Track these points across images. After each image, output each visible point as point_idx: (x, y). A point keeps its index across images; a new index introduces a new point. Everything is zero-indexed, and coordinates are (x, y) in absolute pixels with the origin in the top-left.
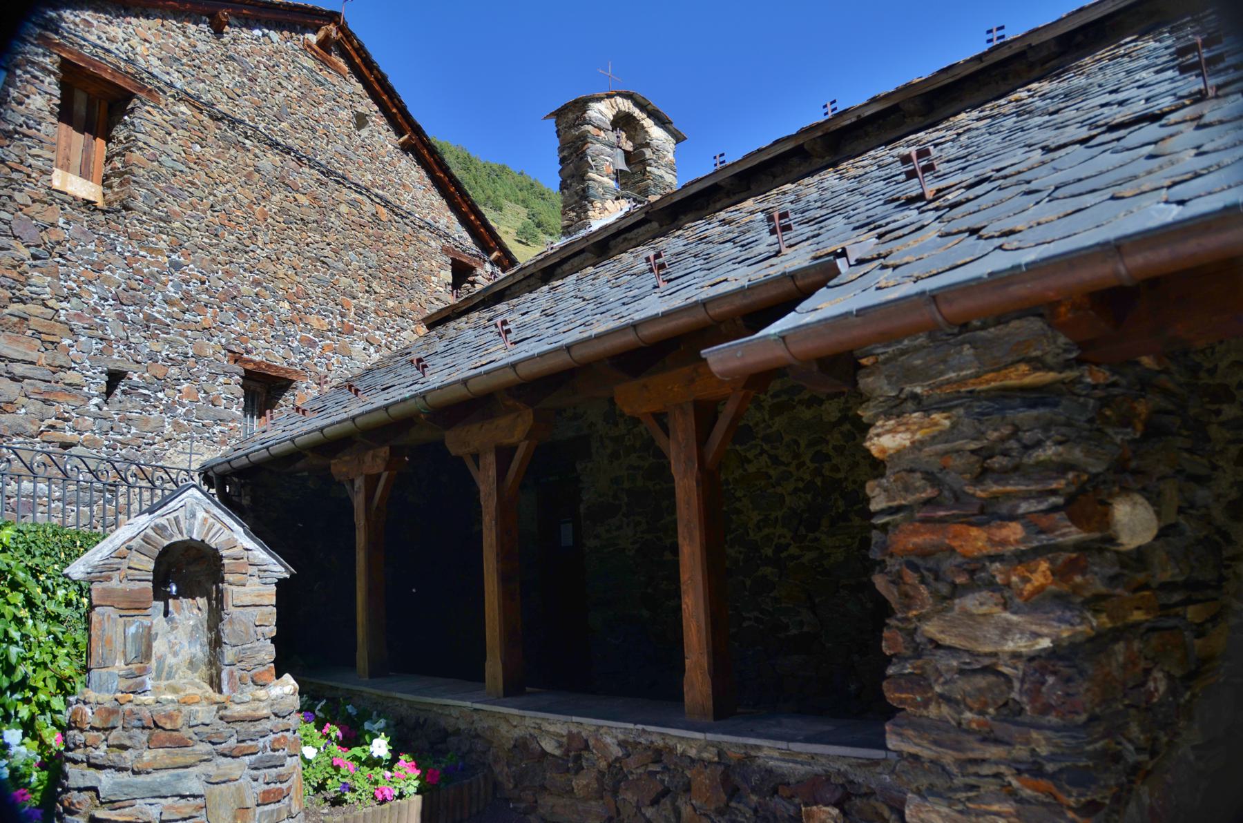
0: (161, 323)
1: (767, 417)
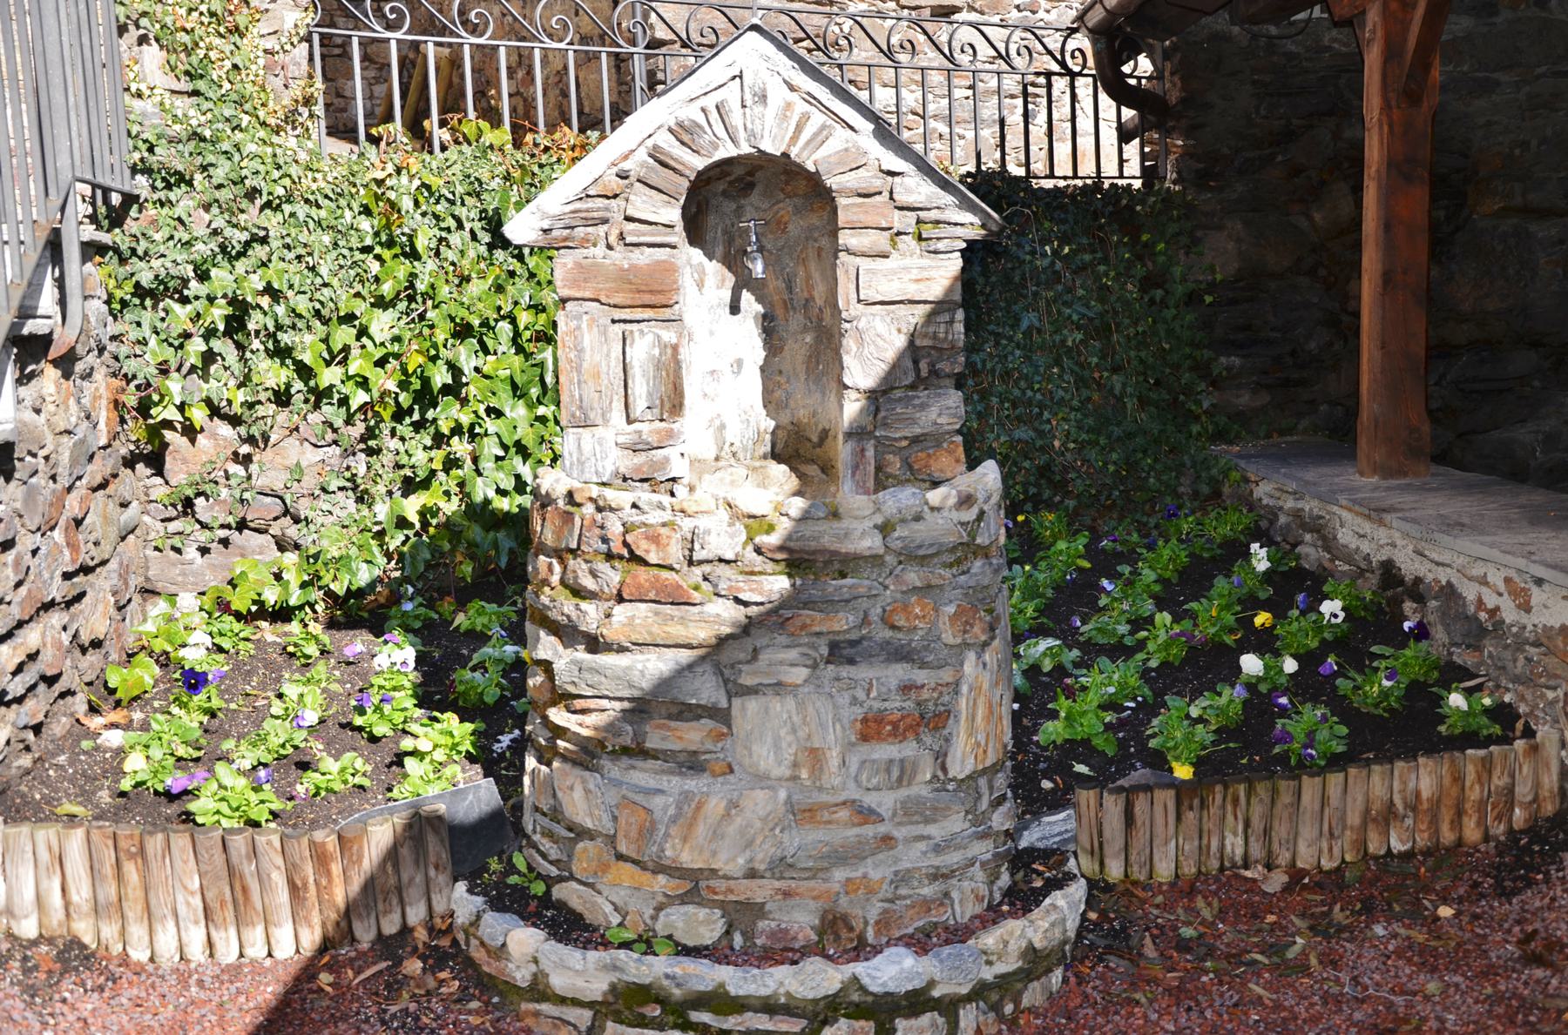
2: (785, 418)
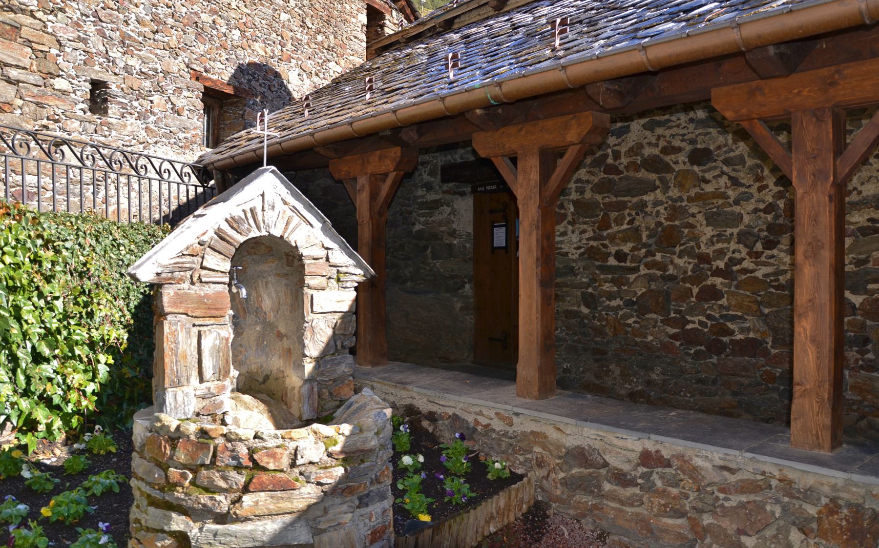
0: (135, 41)
1: (730, 142)
2: (244, 370)
